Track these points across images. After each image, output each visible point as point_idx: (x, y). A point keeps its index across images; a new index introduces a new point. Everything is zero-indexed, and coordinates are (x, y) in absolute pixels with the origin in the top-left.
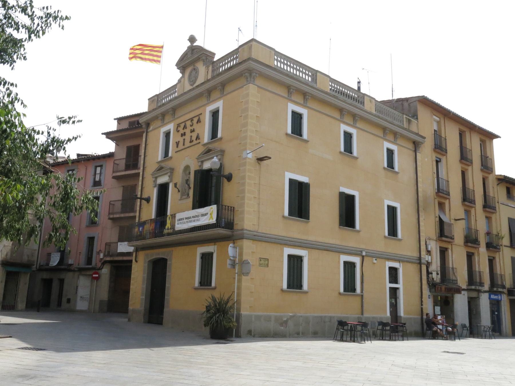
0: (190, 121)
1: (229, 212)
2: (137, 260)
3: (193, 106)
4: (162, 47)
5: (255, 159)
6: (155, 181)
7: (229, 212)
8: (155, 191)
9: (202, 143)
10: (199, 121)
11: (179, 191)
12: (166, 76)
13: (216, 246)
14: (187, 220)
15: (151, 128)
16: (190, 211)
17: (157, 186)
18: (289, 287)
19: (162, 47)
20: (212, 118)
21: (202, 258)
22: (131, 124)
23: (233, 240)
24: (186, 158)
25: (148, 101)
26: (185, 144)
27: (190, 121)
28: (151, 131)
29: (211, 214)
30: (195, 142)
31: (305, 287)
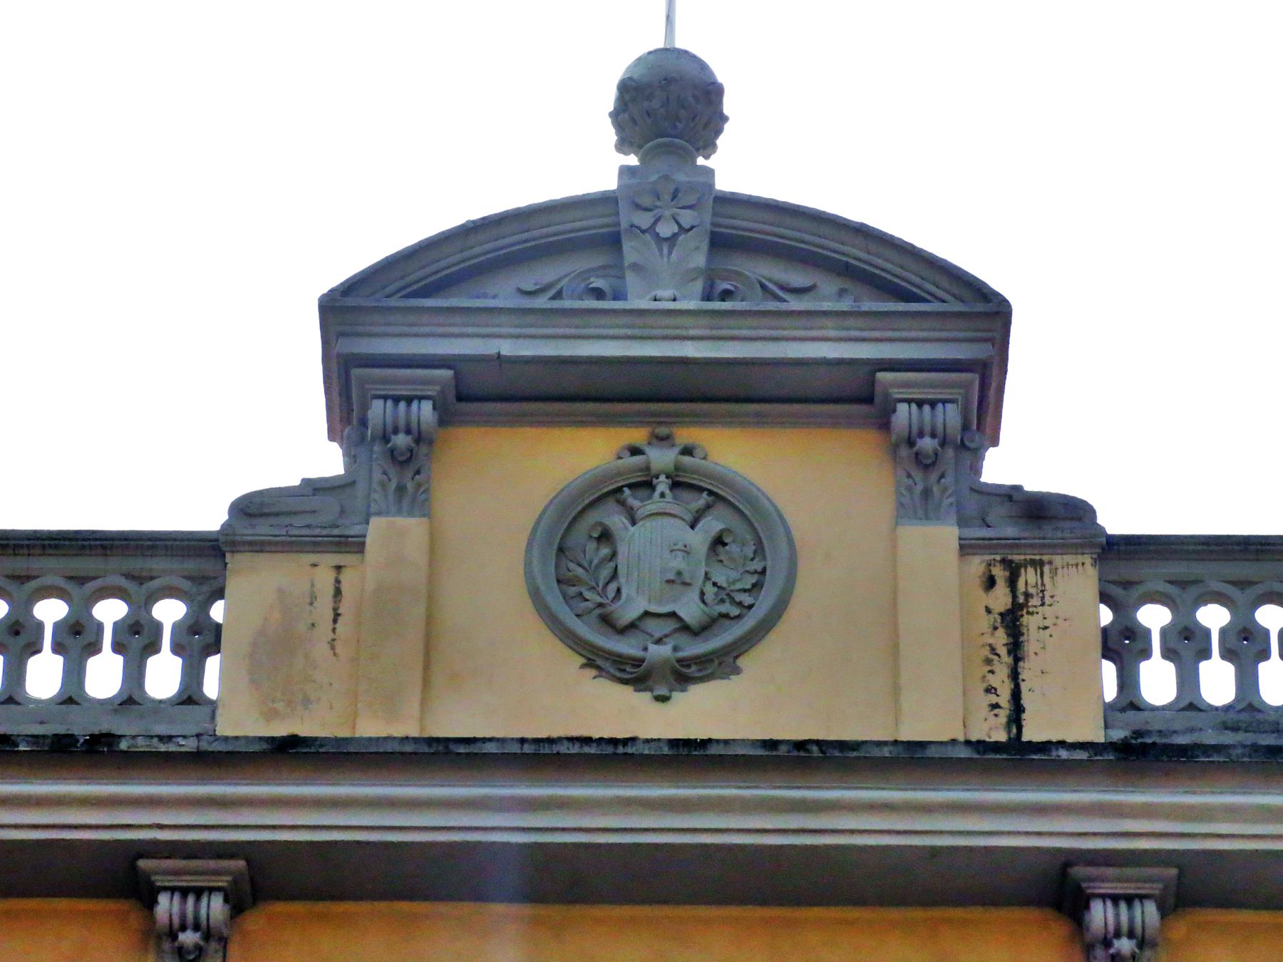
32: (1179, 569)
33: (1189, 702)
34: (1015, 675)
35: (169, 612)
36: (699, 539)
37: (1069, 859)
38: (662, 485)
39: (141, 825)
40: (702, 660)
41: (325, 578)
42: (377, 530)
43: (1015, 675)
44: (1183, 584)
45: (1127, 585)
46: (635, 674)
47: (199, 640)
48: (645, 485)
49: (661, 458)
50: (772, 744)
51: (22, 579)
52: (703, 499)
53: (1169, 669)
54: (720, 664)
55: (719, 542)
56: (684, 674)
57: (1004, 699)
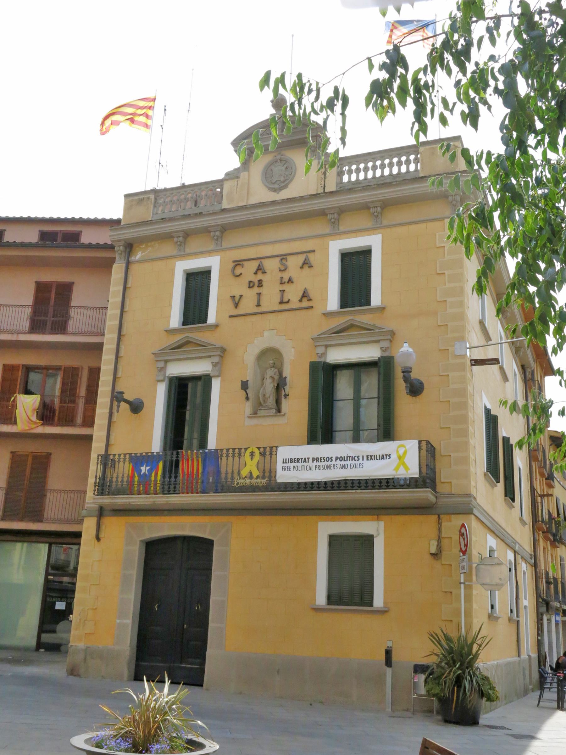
0: (278, 259)
1: (230, 459)
2: (101, 535)
3: (303, 230)
4: (154, 100)
5: (408, 365)
6: (162, 369)
7: (230, 459)
8: (161, 394)
9: (318, 310)
10: (306, 264)
11: (247, 398)
12: (199, 151)
13: (382, 524)
14: (315, 463)
15: (138, 256)
16: (347, 445)
17: (167, 380)
18: (330, 599)
19: (154, 100)
20: (185, 283)
21: (330, 544)
22: (45, 237)
23: (378, 515)
24: (266, 334)
25: (122, 200)
26: (262, 303)
27: (278, 259)
28: (138, 262)
29: (400, 458)
30: (295, 304)
31: (378, 601)
32: (405, 151)
33: (408, 171)
34: (325, 182)
35: (412, 157)
36: (283, 168)
37: (324, 209)
38: (279, 161)
39: (207, 224)
40: (283, 187)
41: (236, 182)
42: (242, 175)
43: (325, 182)
44: (349, 163)
45: (342, 164)
46: (274, 190)
47: (416, 161)
48: (276, 162)
49: (278, 157)
50: (284, 200)
51: (391, 156)
52: (284, 162)
53: (397, 167)
54: (285, 187)
55: (286, 168)
56: (281, 189)
57: (323, 185)
